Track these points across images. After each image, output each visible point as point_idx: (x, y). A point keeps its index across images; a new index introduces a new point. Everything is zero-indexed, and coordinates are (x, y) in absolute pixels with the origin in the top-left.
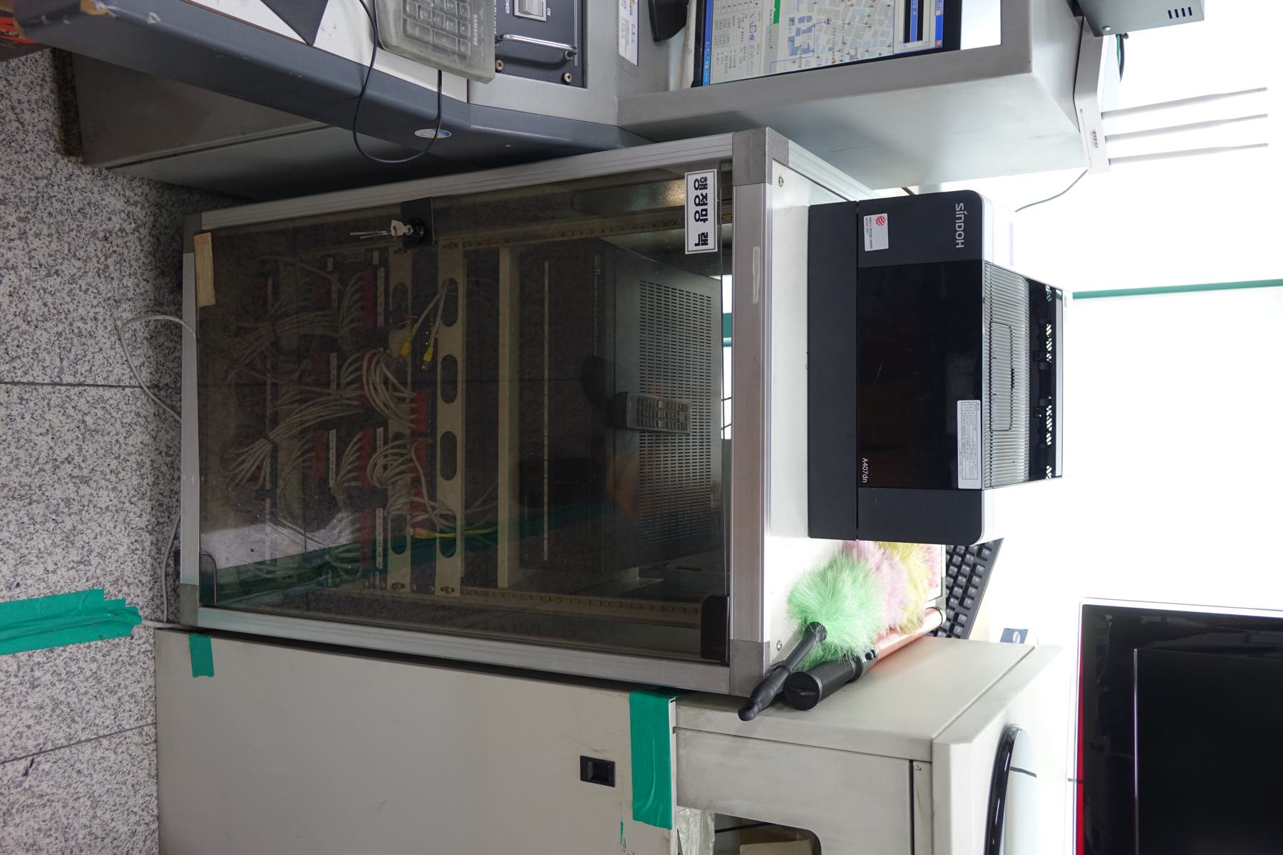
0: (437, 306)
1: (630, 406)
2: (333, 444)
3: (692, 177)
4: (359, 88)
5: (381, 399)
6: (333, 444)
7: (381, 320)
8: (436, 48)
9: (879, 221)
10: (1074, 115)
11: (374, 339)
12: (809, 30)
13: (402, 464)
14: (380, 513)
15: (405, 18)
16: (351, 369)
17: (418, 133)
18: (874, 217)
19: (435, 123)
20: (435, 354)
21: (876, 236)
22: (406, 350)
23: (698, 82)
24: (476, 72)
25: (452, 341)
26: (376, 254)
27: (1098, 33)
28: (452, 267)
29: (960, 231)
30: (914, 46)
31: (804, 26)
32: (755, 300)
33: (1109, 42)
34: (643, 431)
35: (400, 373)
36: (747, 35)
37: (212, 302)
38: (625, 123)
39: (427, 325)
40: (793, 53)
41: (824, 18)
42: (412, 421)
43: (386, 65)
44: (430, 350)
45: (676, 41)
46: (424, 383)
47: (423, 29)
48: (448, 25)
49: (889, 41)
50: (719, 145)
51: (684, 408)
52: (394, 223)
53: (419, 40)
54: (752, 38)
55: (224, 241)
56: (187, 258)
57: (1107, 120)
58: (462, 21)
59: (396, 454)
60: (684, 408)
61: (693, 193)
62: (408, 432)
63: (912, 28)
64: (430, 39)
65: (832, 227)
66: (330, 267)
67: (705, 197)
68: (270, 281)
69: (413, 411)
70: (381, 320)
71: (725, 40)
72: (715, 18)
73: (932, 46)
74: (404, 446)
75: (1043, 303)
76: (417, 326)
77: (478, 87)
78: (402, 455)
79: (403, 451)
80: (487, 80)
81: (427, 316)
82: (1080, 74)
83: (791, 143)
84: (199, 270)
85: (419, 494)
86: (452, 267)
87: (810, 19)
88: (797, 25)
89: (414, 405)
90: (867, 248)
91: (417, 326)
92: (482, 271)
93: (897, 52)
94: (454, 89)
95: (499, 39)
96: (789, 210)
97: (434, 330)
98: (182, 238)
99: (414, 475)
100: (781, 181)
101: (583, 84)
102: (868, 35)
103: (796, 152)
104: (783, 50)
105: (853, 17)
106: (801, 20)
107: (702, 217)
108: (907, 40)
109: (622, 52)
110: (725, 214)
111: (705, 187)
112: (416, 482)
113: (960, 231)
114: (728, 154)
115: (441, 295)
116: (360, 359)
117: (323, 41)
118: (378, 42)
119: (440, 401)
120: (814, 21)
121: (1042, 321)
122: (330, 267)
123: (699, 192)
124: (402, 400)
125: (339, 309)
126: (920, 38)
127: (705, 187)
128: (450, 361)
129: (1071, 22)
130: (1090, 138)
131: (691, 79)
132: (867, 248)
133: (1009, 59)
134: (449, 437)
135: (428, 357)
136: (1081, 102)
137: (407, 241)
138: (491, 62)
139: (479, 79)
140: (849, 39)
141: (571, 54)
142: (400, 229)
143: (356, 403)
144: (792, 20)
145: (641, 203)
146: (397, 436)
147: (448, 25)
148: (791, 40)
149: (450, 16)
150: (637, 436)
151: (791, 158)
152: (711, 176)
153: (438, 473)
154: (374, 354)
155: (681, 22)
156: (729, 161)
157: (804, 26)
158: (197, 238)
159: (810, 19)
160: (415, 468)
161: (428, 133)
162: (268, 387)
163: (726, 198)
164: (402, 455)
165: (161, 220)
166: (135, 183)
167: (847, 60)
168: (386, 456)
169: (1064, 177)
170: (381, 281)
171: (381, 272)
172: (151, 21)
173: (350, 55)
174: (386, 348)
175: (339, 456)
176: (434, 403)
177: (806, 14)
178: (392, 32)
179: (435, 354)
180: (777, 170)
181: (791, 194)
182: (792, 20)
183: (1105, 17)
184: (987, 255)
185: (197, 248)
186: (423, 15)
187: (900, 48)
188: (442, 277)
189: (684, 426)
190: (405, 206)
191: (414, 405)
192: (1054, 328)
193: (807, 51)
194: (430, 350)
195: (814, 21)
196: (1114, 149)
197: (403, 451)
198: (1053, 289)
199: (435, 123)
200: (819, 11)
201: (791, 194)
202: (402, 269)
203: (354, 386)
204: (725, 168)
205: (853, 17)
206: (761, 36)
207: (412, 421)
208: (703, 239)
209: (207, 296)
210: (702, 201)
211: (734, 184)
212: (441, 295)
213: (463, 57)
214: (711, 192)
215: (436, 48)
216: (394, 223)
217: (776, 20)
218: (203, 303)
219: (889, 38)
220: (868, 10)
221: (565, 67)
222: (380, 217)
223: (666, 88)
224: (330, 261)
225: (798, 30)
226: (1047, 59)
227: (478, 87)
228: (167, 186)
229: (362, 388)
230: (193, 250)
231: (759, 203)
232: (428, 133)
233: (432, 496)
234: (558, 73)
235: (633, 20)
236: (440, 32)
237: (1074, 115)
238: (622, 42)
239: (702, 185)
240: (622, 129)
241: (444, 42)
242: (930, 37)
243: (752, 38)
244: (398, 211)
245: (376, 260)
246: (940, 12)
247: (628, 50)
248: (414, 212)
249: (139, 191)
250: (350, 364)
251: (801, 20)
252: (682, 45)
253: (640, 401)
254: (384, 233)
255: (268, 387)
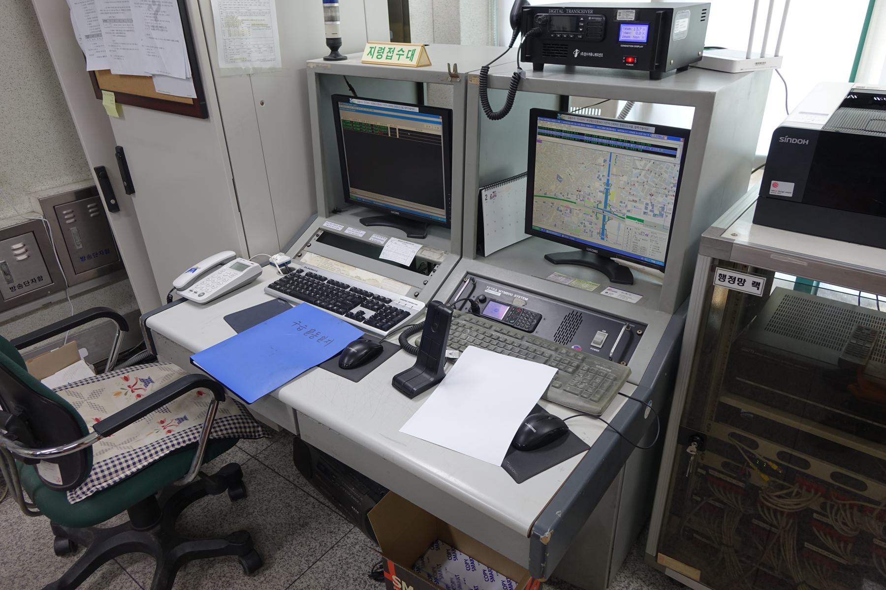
0: (743, 449)
1: (849, 359)
2: (815, 548)
3: (717, 281)
4: (617, 435)
5: (790, 504)
6: (815, 548)
7: (741, 484)
8: (607, 390)
9: (775, 186)
10: (743, 73)
11: (752, 494)
12: (653, 205)
13: (845, 511)
14: (876, 541)
15: (589, 399)
16: (766, 512)
17: (646, 417)
18: (772, 188)
19: (644, 405)
20: (774, 462)
21: (784, 189)
22: (766, 478)
23: (662, 269)
24: (625, 375)
25: (768, 450)
26: (699, 470)
27: (700, 58)
28: (722, 432)
29: (797, 141)
30: (679, 154)
31: (650, 207)
32: (805, 264)
33: (706, 53)
34: (870, 358)
35: (782, 487)
36: (645, 237)
37: (699, 572)
38: (672, 310)
39: (753, 459)
40: (662, 215)
41: (649, 197)
42: (816, 494)
43: (610, 416)
44: (770, 463)
45: (635, 274)
46: (789, 476)
47: (597, 392)
48: (598, 381)
49: (672, 165)
50: (702, 265)
51: (860, 329)
52: (688, 450)
53: (601, 397)
54: (647, 235)
55: (665, 547)
56: (668, 573)
57: (752, 57)
58: (598, 373)
59: (836, 515)
60: (860, 329)
61: (726, 283)
62: (822, 500)
63: (669, 152)
64: (602, 391)
65: (769, 212)
66: (699, 499)
67: (731, 277)
68: (695, 535)
69: (808, 490)
70: (741, 484)
71: (644, 249)
72: (631, 251)
73: (682, 143)
74: (832, 507)
75: (859, 100)
76: (751, 464)
77: (631, 378)
78: (838, 509)
79: (836, 508)
80: (630, 372)
81: (749, 457)
82: (722, 69)
83: (714, 225)
84: (677, 570)
85: (872, 510)
86: (722, 432)
87: (647, 204)
88: (648, 211)
89: (805, 487)
90: (791, 195)
91: (751, 464)
92: (728, 415)
93: (679, 162)
94: (630, 390)
95: (611, 359)
96: (751, 233)
97: (758, 456)
98: (656, 570)
99: (855, 509)
100: (734, 235)
101: (645, 326)
102: (665, 176)
103: (718, 224)
104: (658, 221)
105: (653, 182)
106: (646, 208)
107: (742, 282)
108: (674, 156)
109: (635, 302)
110: (743, 268)
111: (725, 276)
112: (862, 509)
113: (797, 141)
114: (709, 259)
115: (736, 443)
116: (763, 505)
117: (590, 442)
118: (597, 416)
119: (807, 472)
120: (649, 202)
121: (870, 102)
122: (699, 499)
123: (727, 280)
124: (798, 494)
125: (725, 504)
126: (676, 149)
127: (725, 276)
128: (780, 455)
129: (690, 71)
130: (759, 66)
131: (658, 271)
132: (791, 195)
133: (704, 104)
134: (834, 475)
135: (775, 467)
136: (737, 69)
137: (700, 448)
138: (621, 366)
139: (628, 375)
140: (664, 186)
141: (628, 327)
142: (692, 449)
143: (791, 521)
144: (645, 213)
145: (716, 321)
146: (823, 506)
147: (598, 381)
148: (655, 215)
149: (594, 378)
150: (871, 361)
151: (722, 227)
152: (720, 271)
153: (861, 493)
154: (764, 498)
155: (626, 269)
156: (714, 259)
157: (650, 207)
158: (659, 561)
159: (647, 204)
160: (850, 504)
161: (648, 411)
162: (761, 568)
163: (734, 266)
164: (838, 509)
165: (642, 576)
166: (618, 579)
167: (675, 189)
168: (836, 520)
169: (775, 82)
170: (716, 474)
171: (711, 472)
172: (560, 515)
173: (599, 432)
174: (759, 488)
175: (827, 549)
176: (808, 476)
177: (644, 205)
178: (595, 408)
179: (774, 462)
180: (727, 235)
181: (741, 229)
182: (645, 213)
183: (694, 54)
184: (819, 128)
185: (664, 564)
186: (590, 390)
187: (678, 160)
188: (726, 439)
189: (874, 333)
190: (679, 442)
191: (805, 487)
192: (877, 95)
193: (663, 208)
194: (770, 463)
195: (649, 202)
196: (770, 52)
197: (836, 508)
198: (850, 94)
199: (644, 405)
200: (644, 198)
201: (741, 229)
202: (714, 460)
203: (779, 517)
204: (717, 263)
205: (653, 182)
206: (648, 230)
207: (816, 494)
208: (756, 284)
209: (695, 574)
210: (732, 279)
211: (727, 259)
212: (736, 443)
213: (615, 379)
214: (728, 273)
215: (607, 390)
216: (688, 450)
217: (642, 221)
218: (698, 577)
219: (671, 166)
220: (653, 174)
221: (635, 332)
222: (682, 459)
223: (661, 286)
224: (695, 497)
225: (651, 211)
226: (705, 84)
227: (631, 378)
228: (625, 563)
229: (782, 513)
230: (665, 567)
231: (743, 248)
232: (648, 411)
233: (878, 503)
234: (636, 336)
235: (620, 292)
236: (600, 385)
237: (743, 73)
238: (629, 300)
239: (723, 277)
240: (674, 313)
241: (606, 385)
242: (678, 144)
243: (647, 235)
244: (680, 446)
245: (704, 472)
246: (666, 137)
247: (634, 298)
248: (685, 437)
249: (623, 579)
250: (763, 511)
251: (646, 208)
252: (639, 273)
253: (847, 352)
254: (692, 458)
255: (761, 568)
